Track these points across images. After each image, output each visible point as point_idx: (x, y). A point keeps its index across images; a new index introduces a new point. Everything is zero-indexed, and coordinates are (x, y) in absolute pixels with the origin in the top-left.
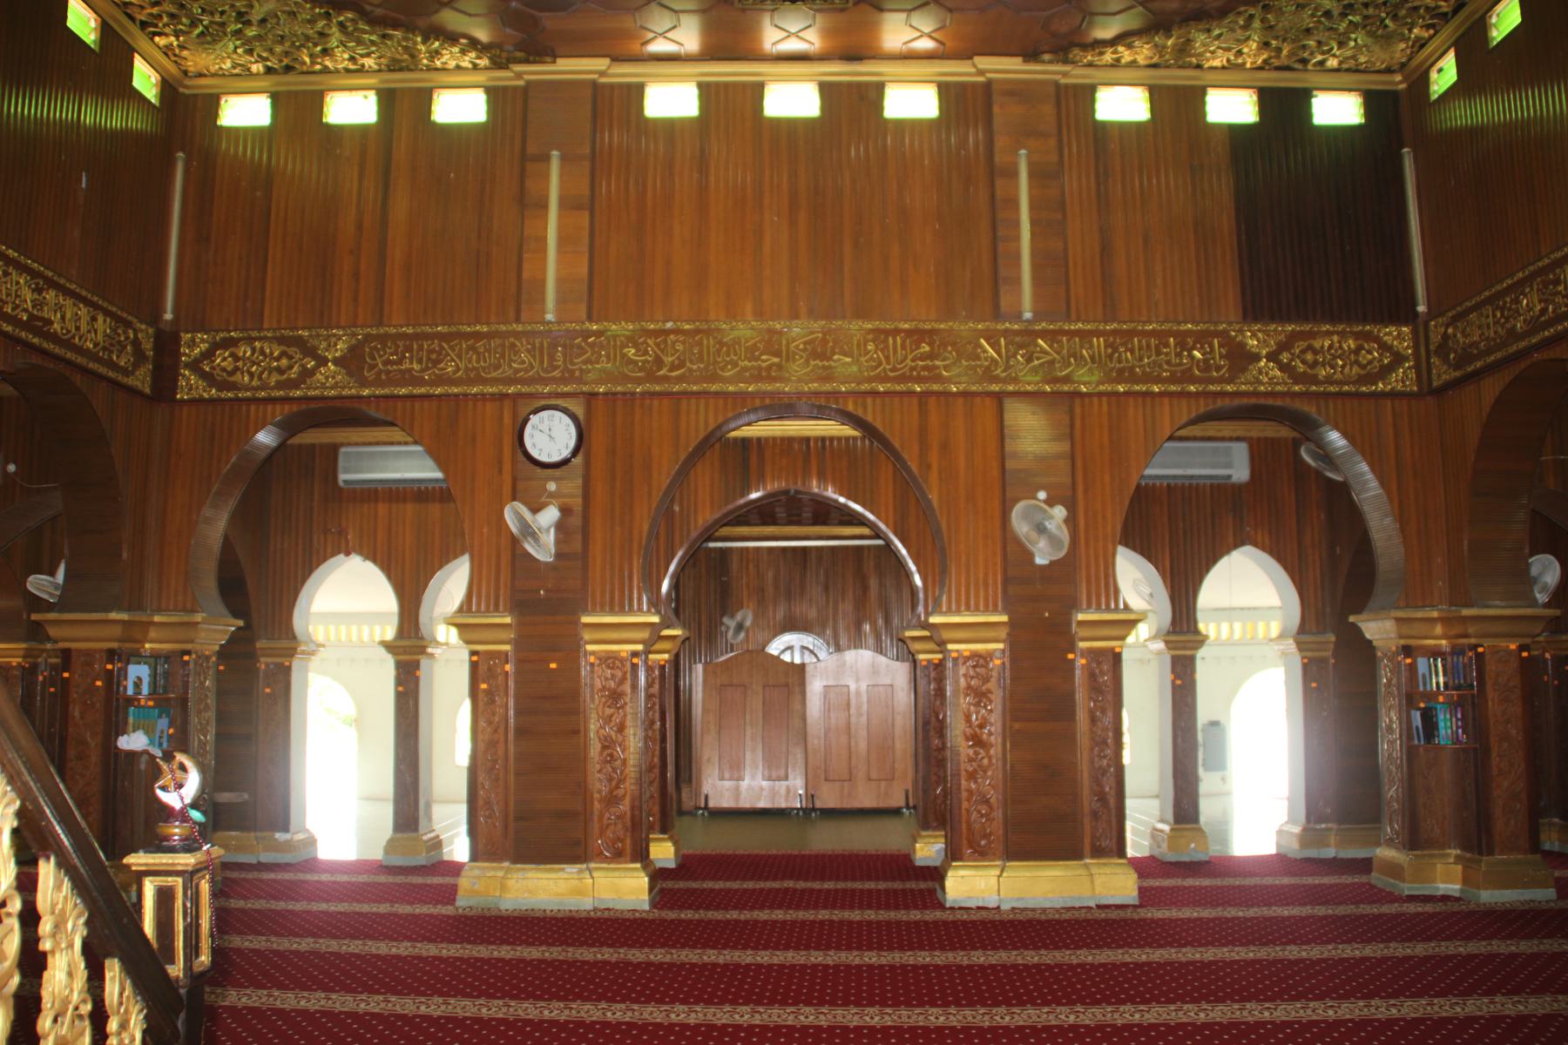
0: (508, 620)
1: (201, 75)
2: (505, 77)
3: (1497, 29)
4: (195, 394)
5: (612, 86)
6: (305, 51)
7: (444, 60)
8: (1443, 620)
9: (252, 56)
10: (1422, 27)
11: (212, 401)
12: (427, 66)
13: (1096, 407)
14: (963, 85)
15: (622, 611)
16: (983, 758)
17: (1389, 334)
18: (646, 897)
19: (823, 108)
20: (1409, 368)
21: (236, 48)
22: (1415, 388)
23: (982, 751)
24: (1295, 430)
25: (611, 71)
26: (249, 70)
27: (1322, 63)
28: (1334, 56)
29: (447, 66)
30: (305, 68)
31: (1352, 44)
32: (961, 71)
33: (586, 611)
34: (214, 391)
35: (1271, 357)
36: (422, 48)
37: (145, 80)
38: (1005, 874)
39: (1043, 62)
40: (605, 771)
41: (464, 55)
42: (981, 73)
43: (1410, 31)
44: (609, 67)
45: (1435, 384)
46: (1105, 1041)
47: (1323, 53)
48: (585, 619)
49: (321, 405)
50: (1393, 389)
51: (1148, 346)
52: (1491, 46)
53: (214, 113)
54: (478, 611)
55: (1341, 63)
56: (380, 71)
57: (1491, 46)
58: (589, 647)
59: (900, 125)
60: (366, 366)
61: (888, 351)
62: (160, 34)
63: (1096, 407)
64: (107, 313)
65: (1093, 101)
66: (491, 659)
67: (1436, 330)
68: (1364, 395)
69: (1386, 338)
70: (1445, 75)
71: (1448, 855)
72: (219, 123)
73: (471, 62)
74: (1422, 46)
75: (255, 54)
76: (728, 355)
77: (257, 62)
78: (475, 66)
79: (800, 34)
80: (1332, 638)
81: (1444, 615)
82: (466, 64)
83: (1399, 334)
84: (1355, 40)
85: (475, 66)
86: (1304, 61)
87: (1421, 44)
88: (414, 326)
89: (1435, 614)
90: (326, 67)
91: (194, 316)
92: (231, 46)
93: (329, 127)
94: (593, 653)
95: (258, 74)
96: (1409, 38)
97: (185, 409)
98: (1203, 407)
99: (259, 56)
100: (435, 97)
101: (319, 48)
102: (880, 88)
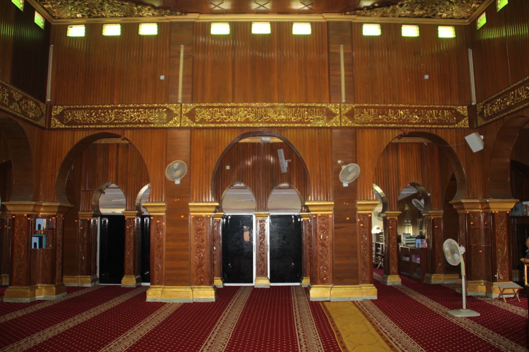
0: (164, 204)
1: (59, 18)
2: (385, 20)
3: (500, 5)
4: (57, 126)
5: (199, 23)
6: (95, 9)
7: (143, 13)
8: (482, 203)
9: (77, 11)
10: (475, 4)
11: (63, 129)
12: (137, 15)
13: (385, 134)
14: (319, 23)
15: (199, 202)
16: (325, 251)
17: (460, 109)
18: (214, 297)
19: (420, 33)
20: (466, 120)
21: (72, 8)
22: (468, 127)
23: (325, 248)
24: (430, 140)
25: (356, 18)
26: (76, 16)
27: (441, 15)
28: (445, 13)
29: (143, 15)
30: (95, 16)
31: (451, 9)
32: (318, 18)
33: (191, 202)
34: (64, 125)
35: (18, 102)
36: (135, 8)
37: (39, 20)
38: (332, 289)
39: (177, 15)
40: (197, 255)
41: (150, 11)
42: (325, 19)
43: (472, 5)
44: (199, 17)
45: (479, 125)
46: (59, 351)
47: (441, 12)
48: (358, 203)
49: (99, 132)
50: (460, 127)
51: (316, 111)
52: (498, 11)
53: (66, 30)
54: (314, 200)
55: (447, 16)
56: (121, 17)
57: (498, 11)
58: (191, 214)
59: (443, 40)
60: (75, 119)
61: (300, 113)
62: (46, 4)
63: (385, 134)
64: (446, 109)
65: (67, 30)
66: (50, 218)
67: (58, 110)
68: (451, 128)
69: (458, 110)
70: (482, 21)
71: (481, 282)
72: (68, 35)
73: (152, 13)
74: (475, 10)
75: (78, 11)
76: (142, 117)
77: (79, 13)
78: (153, 14)
79: (264, 6)
80: (442, 211)
81: (481, 201)
82: (151, 14)
83: (463, 109)
84: (452, 8)
85: (153, 14)
86: (434, 15)
87: (475, 9)
88: (133, 104)
89: (478, 201)
90: (103, 15)
91: (56, 102)
92: (70, 8)
93: (140, 36)
94: (192, 215)
95: (79, 18)
96: (471, 7)
97: (289, 130)
98: (401, 133)
99: (79, 11)
100: (104, 27)
101: (88, 9)
102: (250, 23)
